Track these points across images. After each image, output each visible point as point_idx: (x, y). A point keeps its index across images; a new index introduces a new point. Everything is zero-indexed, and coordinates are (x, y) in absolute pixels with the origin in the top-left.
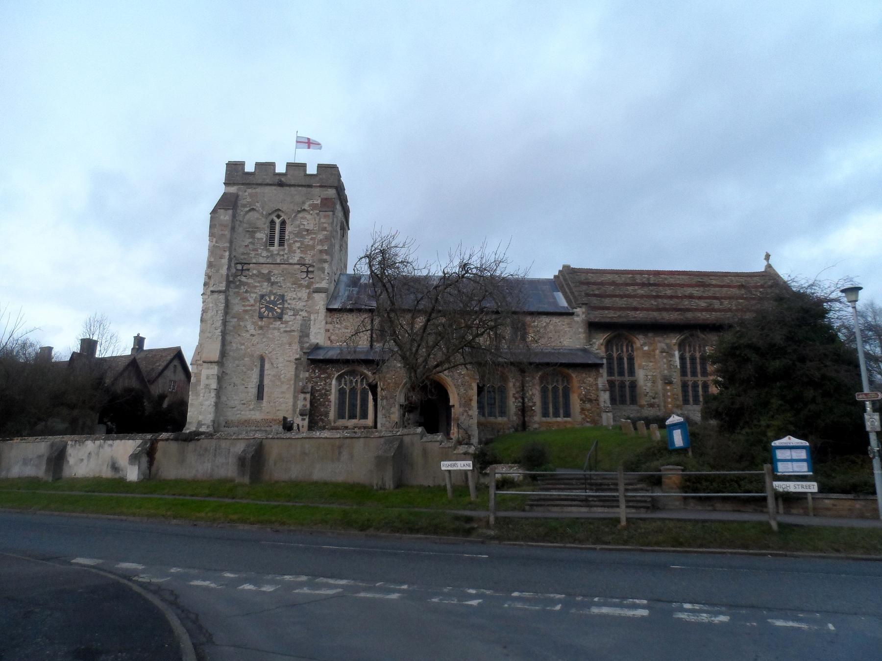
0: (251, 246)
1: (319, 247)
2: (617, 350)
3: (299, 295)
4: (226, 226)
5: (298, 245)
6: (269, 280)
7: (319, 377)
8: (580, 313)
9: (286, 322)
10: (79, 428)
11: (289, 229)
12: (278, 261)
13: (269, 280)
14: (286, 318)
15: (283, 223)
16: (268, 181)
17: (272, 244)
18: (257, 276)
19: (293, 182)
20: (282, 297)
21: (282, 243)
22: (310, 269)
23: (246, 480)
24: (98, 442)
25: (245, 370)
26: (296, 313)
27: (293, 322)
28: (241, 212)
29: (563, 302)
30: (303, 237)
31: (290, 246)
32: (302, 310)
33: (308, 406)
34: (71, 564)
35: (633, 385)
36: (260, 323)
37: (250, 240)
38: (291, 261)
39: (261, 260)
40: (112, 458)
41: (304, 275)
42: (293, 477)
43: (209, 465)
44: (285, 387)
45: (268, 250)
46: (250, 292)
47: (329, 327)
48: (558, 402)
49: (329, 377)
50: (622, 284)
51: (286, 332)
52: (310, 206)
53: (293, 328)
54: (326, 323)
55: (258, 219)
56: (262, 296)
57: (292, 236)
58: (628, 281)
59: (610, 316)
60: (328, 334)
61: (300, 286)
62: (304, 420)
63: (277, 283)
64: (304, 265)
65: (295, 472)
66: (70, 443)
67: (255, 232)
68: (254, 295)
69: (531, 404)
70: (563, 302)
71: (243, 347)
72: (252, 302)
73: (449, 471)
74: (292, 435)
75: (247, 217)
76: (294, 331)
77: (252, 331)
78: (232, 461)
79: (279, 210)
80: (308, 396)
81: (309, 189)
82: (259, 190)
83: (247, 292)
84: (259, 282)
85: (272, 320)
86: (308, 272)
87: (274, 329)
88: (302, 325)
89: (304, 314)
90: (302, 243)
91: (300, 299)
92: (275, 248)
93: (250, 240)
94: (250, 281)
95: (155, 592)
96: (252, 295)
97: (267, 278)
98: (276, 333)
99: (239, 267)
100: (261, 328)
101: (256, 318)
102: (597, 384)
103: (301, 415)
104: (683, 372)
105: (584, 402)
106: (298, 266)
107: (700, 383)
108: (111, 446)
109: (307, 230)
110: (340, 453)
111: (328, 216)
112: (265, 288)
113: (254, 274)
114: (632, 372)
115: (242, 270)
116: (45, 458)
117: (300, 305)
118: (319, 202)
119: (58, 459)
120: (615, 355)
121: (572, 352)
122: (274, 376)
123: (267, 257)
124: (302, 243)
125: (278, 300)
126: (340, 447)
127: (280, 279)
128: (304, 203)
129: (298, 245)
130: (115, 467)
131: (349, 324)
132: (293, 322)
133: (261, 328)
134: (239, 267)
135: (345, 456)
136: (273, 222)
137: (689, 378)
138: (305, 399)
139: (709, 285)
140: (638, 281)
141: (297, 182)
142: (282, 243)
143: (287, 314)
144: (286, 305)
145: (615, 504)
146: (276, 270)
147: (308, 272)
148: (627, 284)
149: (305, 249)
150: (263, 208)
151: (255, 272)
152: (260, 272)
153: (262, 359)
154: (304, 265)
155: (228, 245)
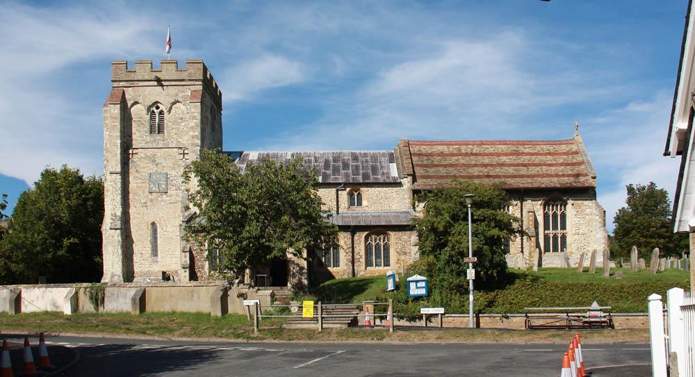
1: (191, 133)
2: (553, 210)
8: (406, 182)
10: (32, 280)
15: (161, 113)
22: (186, 152)
23: (138, 312)
24: (41, 289)
29: (394, 171)
30: (178, 124)
33: (188, 262)
35: (564, 237)
36: (150, 197)
40: (53, 299)
41: (181, 156)
42: (166, 310)
43: (115, 305)
44: (116, 244)
48: (379, 255)
50: (448, 155)
58: (455, 152)
59: (432, 184)
62: (186, 271)
64: (181, 148)
65: (167, 308)
66: (23, 290)
69: (358, 257)
70: (394, 171)
73: (248, 306)
74: (170, 283)
78: (129, 301)
79: (157, 102)
80: (188, 254)
86: (184, 154)
87: (162, 201)
95: (298, 361)
100: (151, 200)
102: (410, 241)
103: (184, 268)
104: (546, 227)
105: (400, 255)
106: (177, 149)
107: (559, 236)
108: (50, 291)
110: (192, 296)
112: (154, 169)
114: (564, 227)
116: (8, 300)
118: (189, 94)
119: (17, 301)
120: (551, 213)
121: (397, 214)
124: (178, 129)
126: (192, 292)
130: (54, 305)
135: (195, 297)
137: (551, 232)
138: (185, 257)
139: (523, 154)
140: (463, 151)
146: (159, 153)
148: (452, 155)
151: (142, 155)
154: (181, 148)
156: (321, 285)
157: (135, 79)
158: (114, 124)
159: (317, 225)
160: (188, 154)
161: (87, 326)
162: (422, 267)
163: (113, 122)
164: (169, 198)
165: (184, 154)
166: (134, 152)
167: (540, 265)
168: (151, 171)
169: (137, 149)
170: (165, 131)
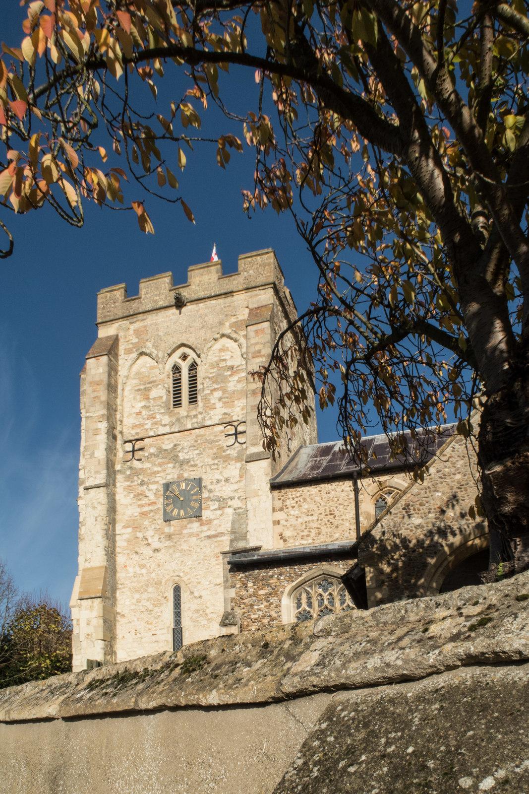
0: (144, 413)
3: (227, 474)
4: (98, 383)
5: (218, 394)
6: (175, 459)
7: (255, 595)
9: (209, 522)
11: (201, 372)
12: (189, 427)
13: (175, 459)
14: (206, 514)
15: (193, 367)
16: (161, 303)
17: (177, 403)
18: (157, 456)
19: (201, 295)
20: (199, 481)
21: (193, 399)
22: (240, 429)
25: (151, 607)
26: (223, 503)
27: (220, 520)
28: (124, 361)
30: (225, 380)
31: (206, 399)
32: (232, 498)
34: (414, 130)
36: (167, 530)
37: (143, 403)
38: (208, 423)
39: (162, 430)
41: (232, 440)
45: (171, 414)
46: (148, 484)
47: (280, 516)
49: (275, 592)
51: (209, 537)
52: (231, 326)
53: (220, 530)
54: (274, 510)
55: (152, 368)
56: (167, 486)
57: (207, 383)
60: (279, 529)
61: (227, 459)
63: (188, 461)
64: (229, 423)
67: (148, 390)
68: (153, 487)
71: (144, 571)
72: (152, 497)
75: (135, 368)
76: (222, 534)
77: (156, 544)
81: (229, 300)
82: (151, 319)
83: (142, 483)
84: (160, 465)
85: (185, 521)
87: (191, 535)
88: (233, 522)
89: (236, 503)
90: (224, 391)
91: (227, 480)
92: (182, 411)
93: (143, 403)
94: (147, 465)
96: (151, 487)
97: (172, 456)
98: (193, 540)
99: (129, 447)
100: (169, 537)
101: (161, 521)
106: (221, 428)
109: (232, 368)
111: (263, 331)
112: (171, 473)
113: (151, 454)
115: (133, 451)
117: (225, 491)
122: (197, 611)
123: (172, 424)
124: (224, 391)
125: (193, 488)
127: (192, 454)
128: (221, 323)
129: (218, 394)
131: (313, 506)
132: (220, 520)
133: (169, 537)
134: (129, 447)
136: (176, 369)
141: (207, 293)
142: (193, 399)
143: (208, 508)
144: (205, 495)
145: (238, 558)
146: (186, 441)
147: (236, 434)
149: (228, 399)
150: (156, 347)
151: (152, 450)
152: (161, 450)
153: (177, 590)
154: (229, 423)
155: (105, 412)
156: (412, 27)
157: (141, 310)
158: (95, 394)
159: (478, 173)
160: (244, 432)
161: (368, 743)
162: (310, 724)
163: (94, 391)
164: (205, 528)
165: (236, 434)
166: (136, 447)
167: (356, 491)
168: (169, 478)
169: (142, 439)
170: (199, 398)
